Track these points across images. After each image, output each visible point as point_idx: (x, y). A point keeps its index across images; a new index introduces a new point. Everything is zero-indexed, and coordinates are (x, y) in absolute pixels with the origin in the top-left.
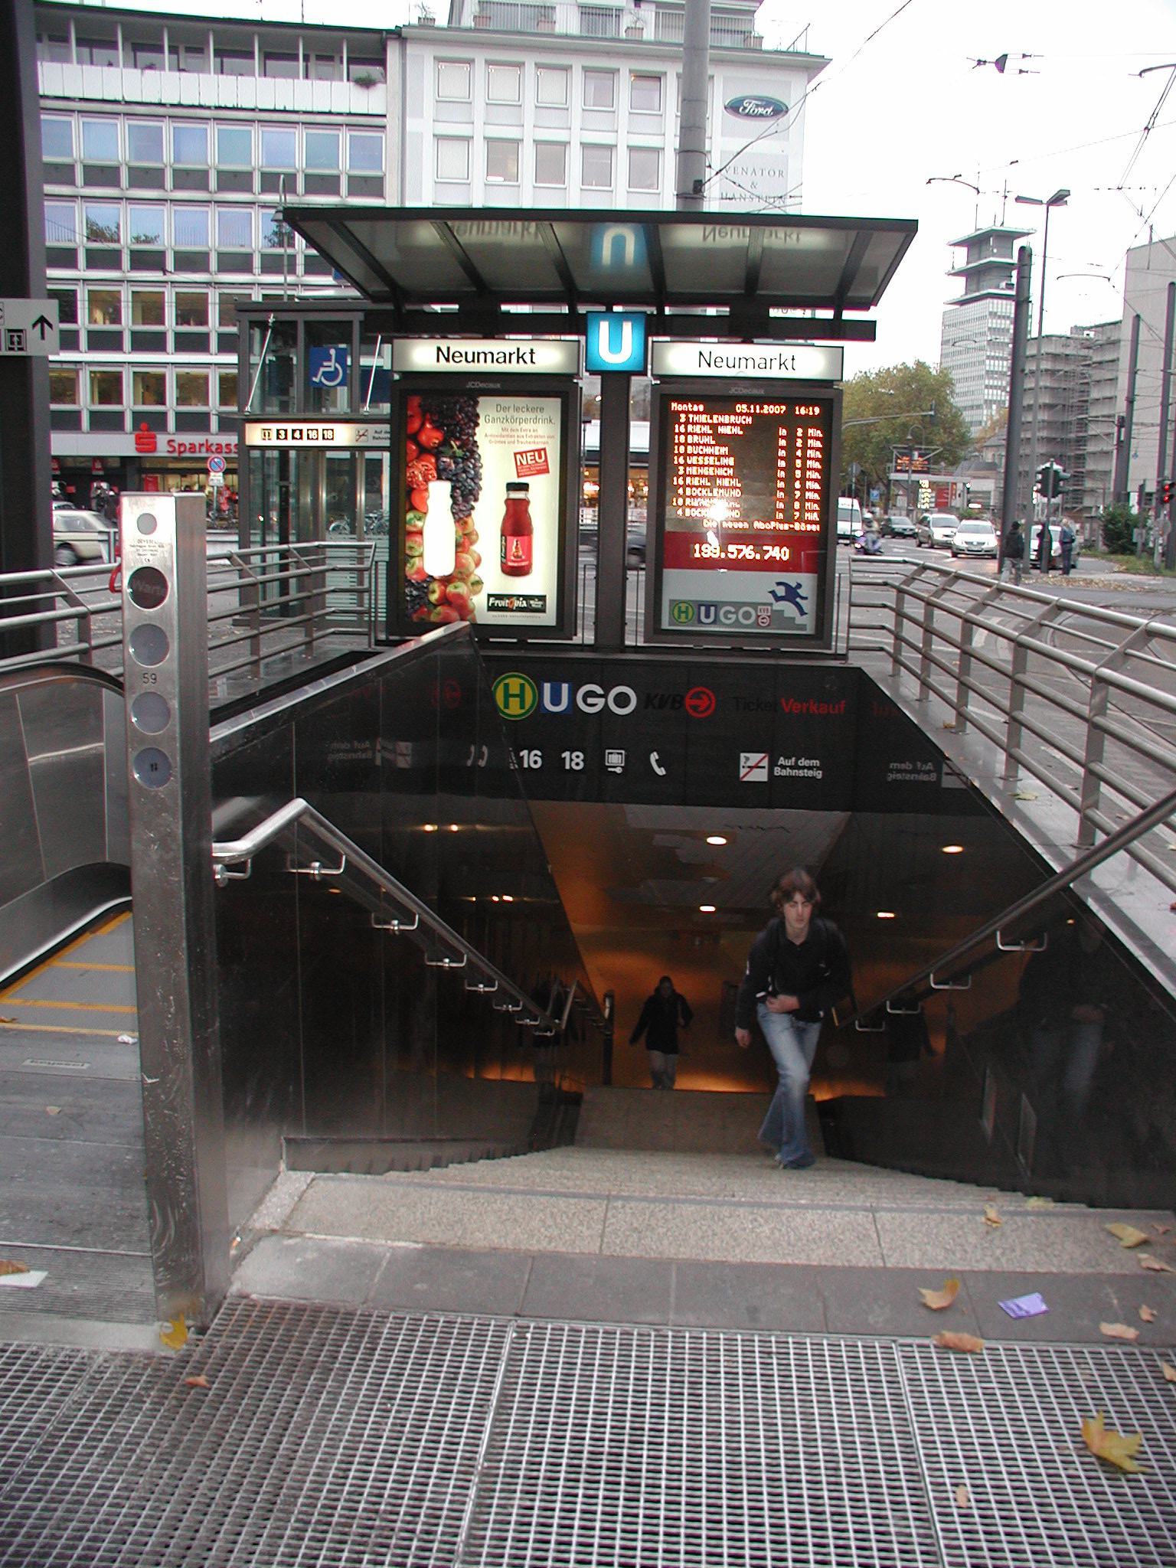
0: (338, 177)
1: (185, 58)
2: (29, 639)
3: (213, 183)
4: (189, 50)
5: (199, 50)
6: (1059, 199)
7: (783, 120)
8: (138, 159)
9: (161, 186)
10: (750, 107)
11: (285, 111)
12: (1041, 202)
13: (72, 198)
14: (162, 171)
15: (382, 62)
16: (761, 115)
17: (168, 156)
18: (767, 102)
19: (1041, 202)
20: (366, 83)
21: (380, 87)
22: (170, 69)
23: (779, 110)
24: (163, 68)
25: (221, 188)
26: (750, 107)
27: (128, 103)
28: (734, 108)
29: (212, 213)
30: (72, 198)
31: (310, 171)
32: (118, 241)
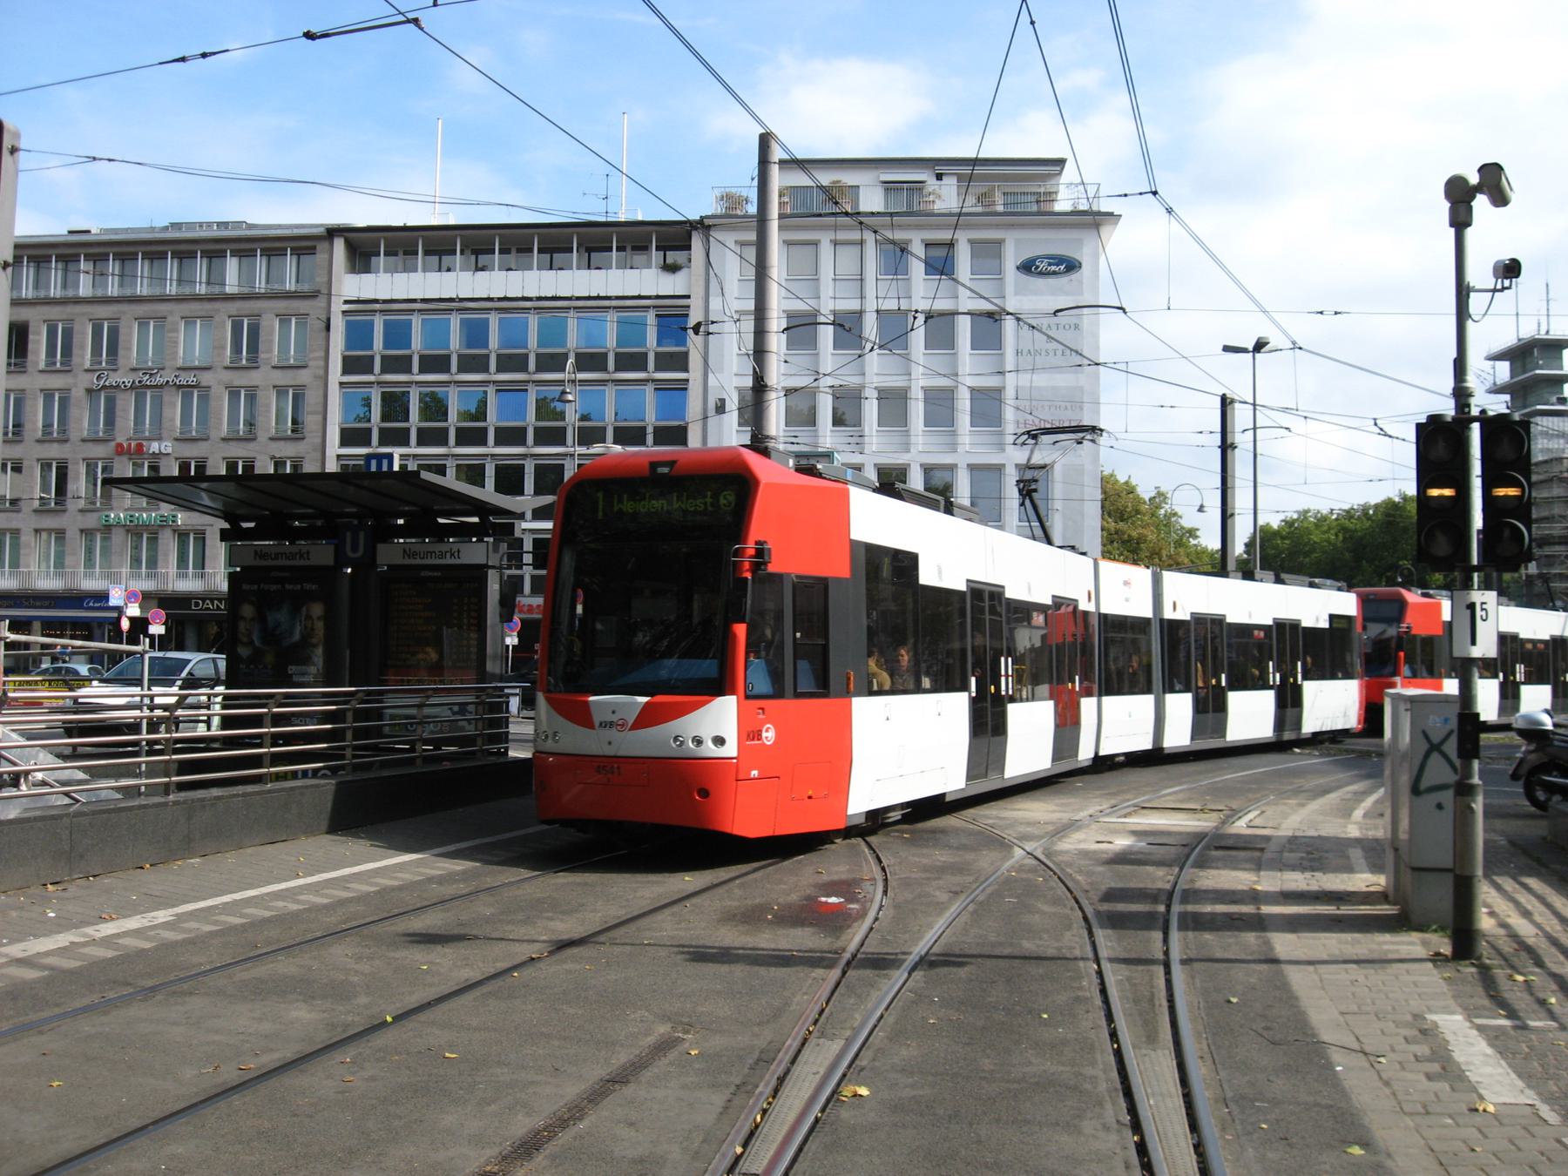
0: (646, 354)
1: (512, 258)
2: (15, 780)
3: (532, 365)
4: (635, 248)
5: (642, 248)
6: (1260, 346)
7: (1074, 276)
8: (469, 346)
9: (604, 369)
10: (1043, 266)
11: (598, 298)
12: (1244, 350)
13: (603, 382)
14: (448, 357)
15: (689, 248)
16: (1054, 273)
17: (494, 342)
18: (1059, 260)
19: (1244, 350)
20: (671, 268)
21: (684, 272)
22: (386, 271)
23: (1072, 266)
24: (416, 270)
25: (539, 369)
26: (1043, 266)
27: (462, 300)
28: (1027, 267)
29: (610, 392)
30: (603, 382)
31: (660, 349)
32: (369, 421)
